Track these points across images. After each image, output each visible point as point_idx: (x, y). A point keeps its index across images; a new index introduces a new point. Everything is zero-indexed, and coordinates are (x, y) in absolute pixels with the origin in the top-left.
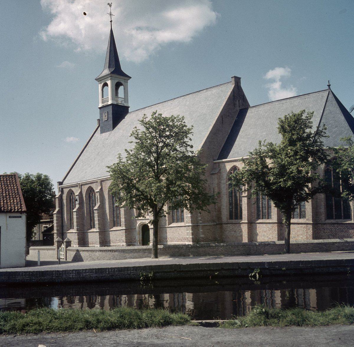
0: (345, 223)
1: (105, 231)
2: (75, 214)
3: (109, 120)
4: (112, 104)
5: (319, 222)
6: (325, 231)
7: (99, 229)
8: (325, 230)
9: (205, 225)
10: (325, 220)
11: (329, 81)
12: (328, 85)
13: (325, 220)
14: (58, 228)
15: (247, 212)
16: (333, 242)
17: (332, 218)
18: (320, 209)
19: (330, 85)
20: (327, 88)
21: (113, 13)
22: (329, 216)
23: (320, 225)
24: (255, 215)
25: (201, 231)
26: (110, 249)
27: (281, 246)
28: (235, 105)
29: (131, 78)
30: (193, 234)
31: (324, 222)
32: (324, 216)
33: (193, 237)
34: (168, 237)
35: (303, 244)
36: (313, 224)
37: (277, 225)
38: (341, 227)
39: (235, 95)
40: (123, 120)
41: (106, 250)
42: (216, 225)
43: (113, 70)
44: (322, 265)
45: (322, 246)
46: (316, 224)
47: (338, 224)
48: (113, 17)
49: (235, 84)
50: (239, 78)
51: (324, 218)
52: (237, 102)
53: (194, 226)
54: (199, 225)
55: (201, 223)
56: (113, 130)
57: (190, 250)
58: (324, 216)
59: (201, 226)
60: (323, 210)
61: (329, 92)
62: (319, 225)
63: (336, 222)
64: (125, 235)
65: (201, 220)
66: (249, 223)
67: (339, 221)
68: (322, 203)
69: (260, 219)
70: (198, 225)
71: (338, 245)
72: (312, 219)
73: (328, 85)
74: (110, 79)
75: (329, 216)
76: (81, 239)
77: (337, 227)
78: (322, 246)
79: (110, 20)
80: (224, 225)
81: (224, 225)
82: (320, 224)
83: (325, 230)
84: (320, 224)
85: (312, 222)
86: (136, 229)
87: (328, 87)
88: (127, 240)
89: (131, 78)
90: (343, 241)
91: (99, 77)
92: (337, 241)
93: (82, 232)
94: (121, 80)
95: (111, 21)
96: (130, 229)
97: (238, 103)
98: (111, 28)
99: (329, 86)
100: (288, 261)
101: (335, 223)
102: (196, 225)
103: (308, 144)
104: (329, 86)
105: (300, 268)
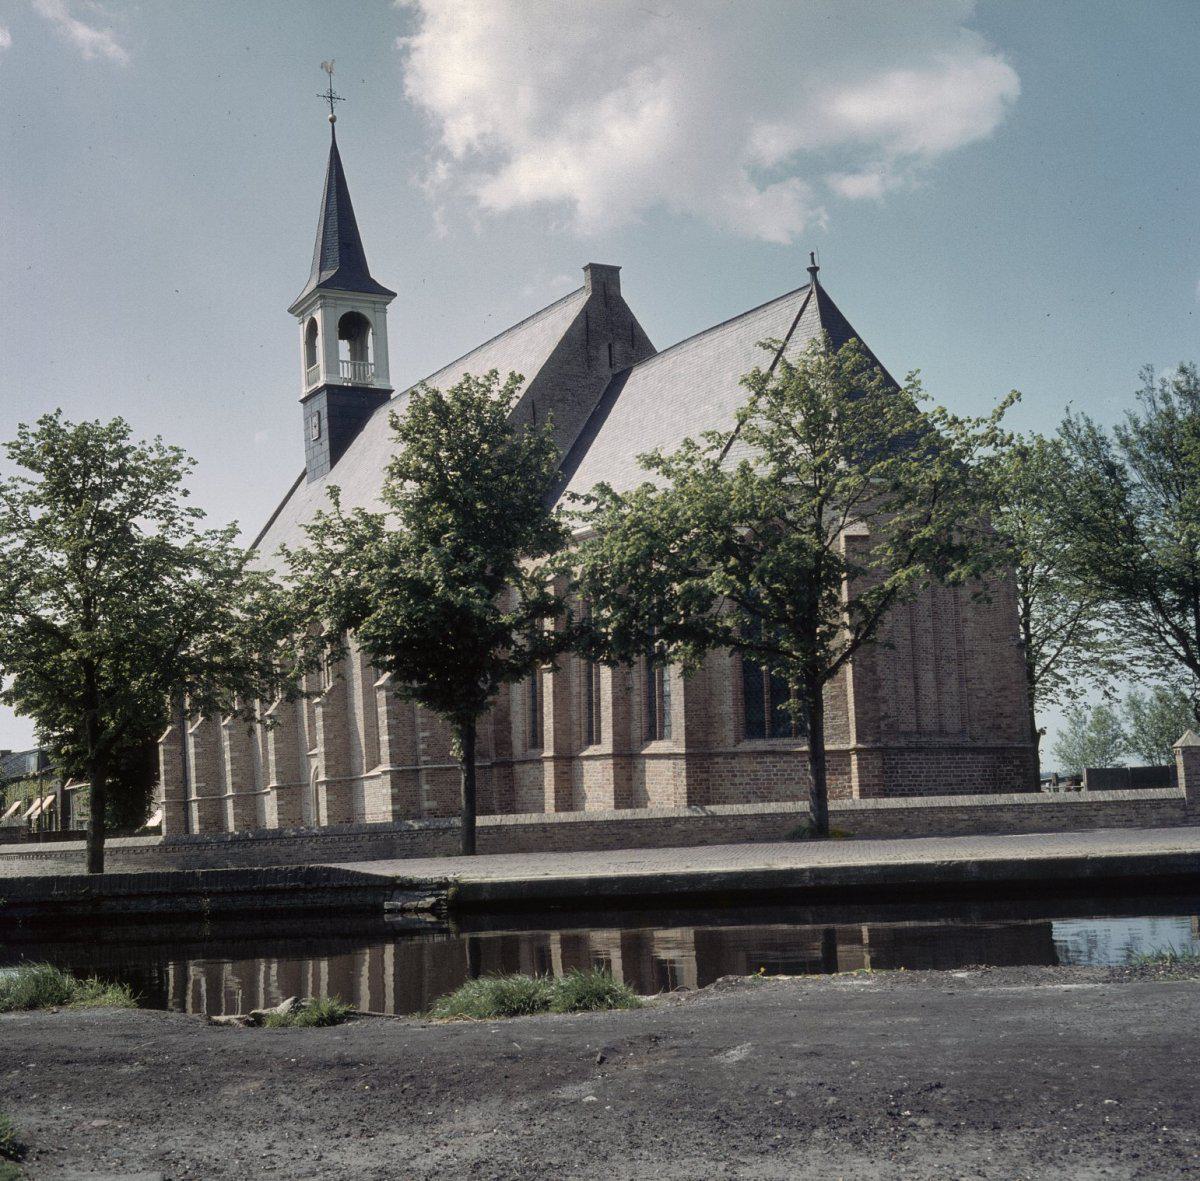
0: (797, 749)
1: (256, 795)
2: (191, 741)
3: (321, 440)
4: (327, 387)
5: (716, 750)
6: (737, 780)
7: (233, 787)
8: (736, 776)
9: (441, 769)
10: (738, 741)
11: (812, 254)
12: (810, 270)
13: (738, 741)
14: (169, 788)
15: (552, 720)
16: (664, 819)
17: (761, 735)
18: (721, 703)
19: (817, 269)
20: (807, 278)
21: (338, 93)
22: (752, 728)
23: (720, 760)
24: (637, 730)
25: (426, 787)
26: (37, 850)
27: (489, 833)
28: (590, 361)
29: (395, 295)
30: (395, 799)
31: (733, 749)
32: (732, 728)
33: (397, 807)
34: (367, 811)
35: (559, 824)
36: (688, 757)
37: (611, 761)
38: (758, 767)
39: (592, 326)
40: (361, 434)
41: (28, 854)
42: (491, 767)
43: (328, 274)
44: (123, 891)
45: (625, 831)
46: (700, 758)
47: (773, 753)
48: (337, 105)
49: (593, 290)
50: (614, 271)
51: (731, 735)
52: (604, 352)
53: (399, 772)
54: (421, 769)
55: (425, 762)
56: (332, 467)
57: (230, 851)
58: (732, 728)
59: (425, 772)
60: (728, 705)
61: (811, 292)
62: (716, 760)
63: (769, 748)
64: (278, 805)
65: (425, 753)
66: (562, 758)
67: (779, 744)
68: (727, 683)
69: (655, 739)
70: (418, 767)
71: (684, 828)
72: (687, 740)
73: (810, 270)
74: (321, 307)
75: (752, 728)
76: (212, 821)
77: (774, 766)
78: (625, 831)
79: (330, 116)
80: (518, 768)
81: (518, 768)
82: (719, 755)
83: (736, 776)
84: (719, 755)
85: (682, 750)
86: (308, 785)
87: (809, 274)
88: (283, 822)
89: (395, 295)
90: (704, 815)
91: (300, 299)
92: (681, 815)
93: (213, 800)
94: (363, 306)
95: (333, 120)
96: (296, 786)
97: (607, 353)
98: (331, 140)
99: (814, 270)
100: (19, 879)
101: (766, 753)
102: (413, 770)
103: (446, 475)
104: (814, 270)
105: (50, 899)
